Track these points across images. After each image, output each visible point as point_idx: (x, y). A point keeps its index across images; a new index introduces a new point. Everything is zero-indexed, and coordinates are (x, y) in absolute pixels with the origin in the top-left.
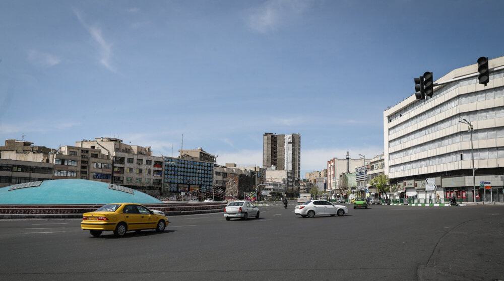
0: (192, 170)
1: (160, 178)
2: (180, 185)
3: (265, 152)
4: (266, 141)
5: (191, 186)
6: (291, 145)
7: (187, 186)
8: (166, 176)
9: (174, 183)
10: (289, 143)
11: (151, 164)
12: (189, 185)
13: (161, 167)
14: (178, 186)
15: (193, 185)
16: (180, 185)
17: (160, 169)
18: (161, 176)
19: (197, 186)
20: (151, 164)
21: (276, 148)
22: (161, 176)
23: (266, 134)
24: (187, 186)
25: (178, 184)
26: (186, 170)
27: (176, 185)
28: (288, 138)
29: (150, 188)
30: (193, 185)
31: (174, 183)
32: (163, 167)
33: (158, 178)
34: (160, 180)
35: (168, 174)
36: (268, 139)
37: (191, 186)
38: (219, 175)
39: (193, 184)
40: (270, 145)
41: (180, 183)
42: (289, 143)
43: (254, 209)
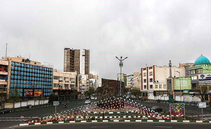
0: (36, 75)
1: (6, 83)
2: (25, 90)
3: (66, 61)
4: (66, 54)
5: (35, 90)
6: (84, 57)
7: (32, 90)
8: (12, 81)
9: (20, 88)
10: (83, 55)
11: (152, 69)
12: (34, 89)
13: (7, 71)
14: (23, 90)
15: (38, 89)
16: (25, 90)
17: (6, 73)
18: (6, 81)
19: (40, 90)
20: (152, 69)
21: (74, 59)
22: (6, 81)
23: (66, 49)
24: (32, 90)
25: (23, 89)
26: (38, 75)
27: (21, 90)
28: (82, 53)
29: (56, 91)
30: (38, 89)
31: (20, 88)
32: (9, 72)
33: (3, 83)
34: (5, 86)
35: (14, 79)
36: (67, 52)
37: (35, 90)
38: (57, 79)
39: (37, 89)
40: (69, 57)
41: (26, 88)
42: (83, 55)
43: (159, 98)
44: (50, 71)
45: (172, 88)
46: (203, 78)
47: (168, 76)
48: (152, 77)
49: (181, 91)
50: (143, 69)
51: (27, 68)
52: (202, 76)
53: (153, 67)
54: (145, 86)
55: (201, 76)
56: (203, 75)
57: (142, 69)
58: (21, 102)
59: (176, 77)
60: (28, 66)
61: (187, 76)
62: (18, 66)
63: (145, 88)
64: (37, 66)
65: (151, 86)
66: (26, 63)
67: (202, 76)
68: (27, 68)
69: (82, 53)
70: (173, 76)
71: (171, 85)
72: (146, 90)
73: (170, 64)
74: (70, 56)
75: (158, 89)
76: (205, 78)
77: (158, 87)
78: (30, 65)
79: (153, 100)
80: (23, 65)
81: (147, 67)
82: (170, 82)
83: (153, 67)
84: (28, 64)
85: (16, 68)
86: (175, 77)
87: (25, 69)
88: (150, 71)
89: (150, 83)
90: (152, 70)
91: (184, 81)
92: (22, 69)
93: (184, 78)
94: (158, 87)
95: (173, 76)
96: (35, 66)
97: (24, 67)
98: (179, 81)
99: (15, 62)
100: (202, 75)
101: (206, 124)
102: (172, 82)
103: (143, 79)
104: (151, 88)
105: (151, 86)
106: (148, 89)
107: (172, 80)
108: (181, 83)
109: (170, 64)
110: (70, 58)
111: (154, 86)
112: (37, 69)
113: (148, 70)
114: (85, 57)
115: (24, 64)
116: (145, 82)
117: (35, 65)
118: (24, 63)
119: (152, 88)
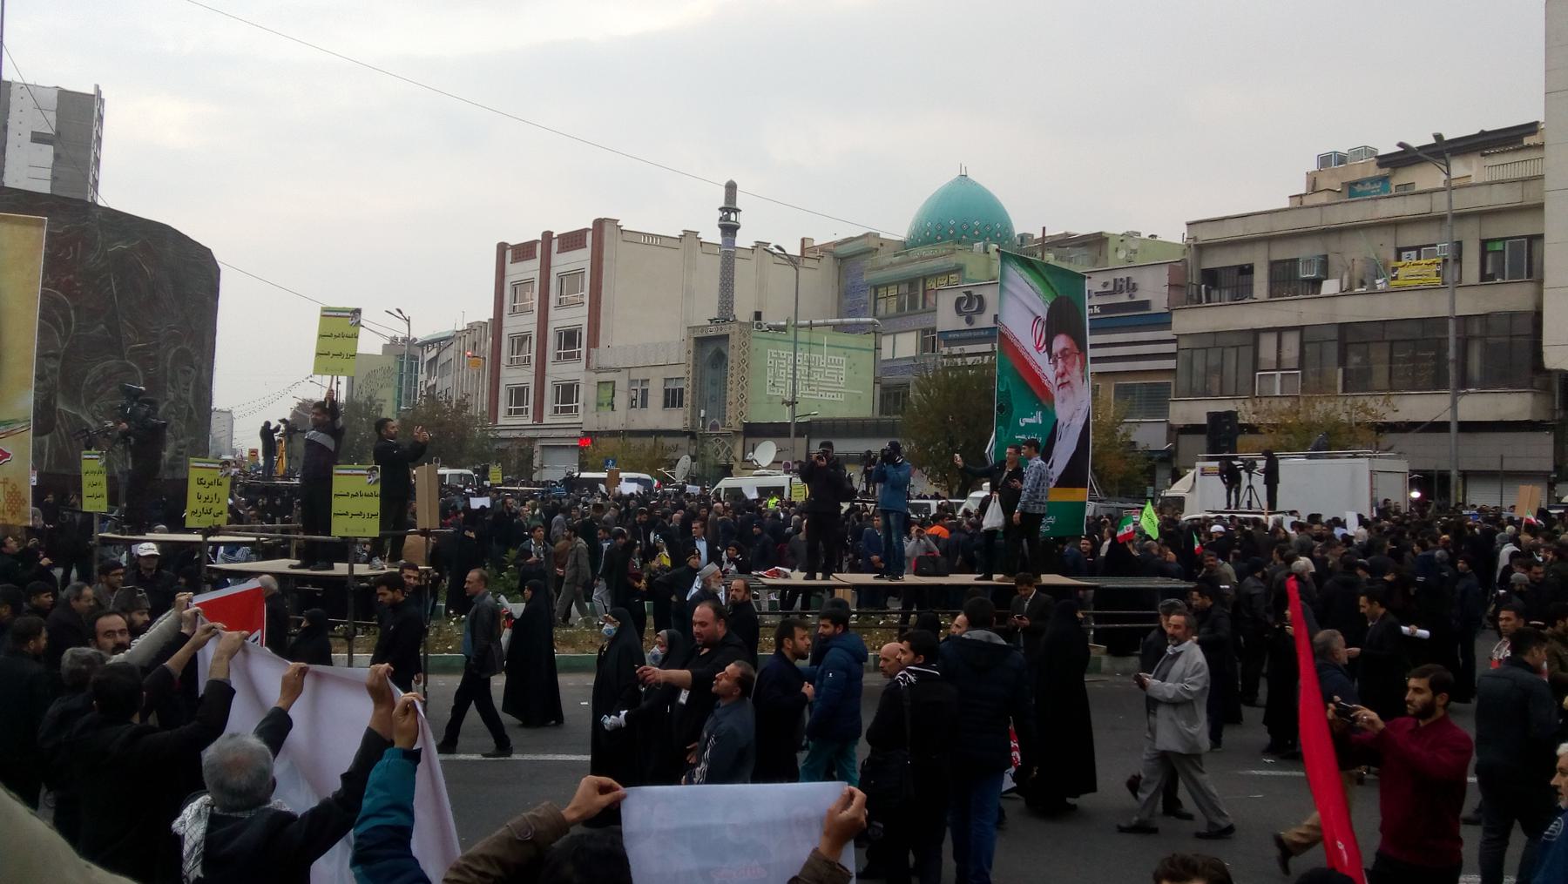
6: (49, 150)
10: (38, 138)
42: (38, 138)
45: (731, 411)
46: (969, 321)
47: (705, 311)
48: (577, 317)
49: (799, 434)
50: (509, 254)
52: (969, 305)
53: (539, 246)
54: (518, 394)
55: (959, 301)
56: (976, 292)
57: (502, 248)
58: (894, 334)
59: (768, 319)
61: (851, 313)
63: (518, 412)
65: (568, 392)
67: (969, 305)
70: (743, 313)
71: (721, 384)
72: (522, 428)
73: (730, 208)
75: (618, 419)
77: (621, 400)
81: (548, 236)
82: (720, 360)
83: (539, 246)
86: (758, 315)
88: (563, 262)
89: (559, 372)
90: (581, 259)
91: (823, 357)
93: (826, 338)
94: (621, 400)
95: (743, 313)
98: (786, 352)
100: (969, 293)
101: (546, 753)
102: (733, 355)
103: (505, 333)
104: (564, 410)
105: (568, 392)
106: (539, 413)
107: (734, 340)
108: (802, 369)
109: (730, 208)
111: (586, 394)
113: (508, 266)
114: (57, 156)
116: (571, 356)
119: (569, 410)
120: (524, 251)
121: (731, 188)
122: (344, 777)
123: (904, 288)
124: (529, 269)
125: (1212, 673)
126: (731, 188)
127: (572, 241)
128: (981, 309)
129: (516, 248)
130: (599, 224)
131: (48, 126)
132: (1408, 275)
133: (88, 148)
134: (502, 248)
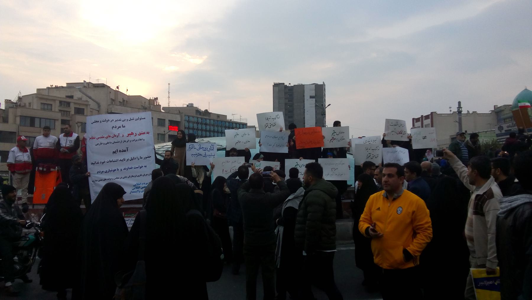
10: (311, 97)
42: (311, 97)
44: (345, 182)
51: (206, 124)
57: (413, 119)
60: (208, 122)
62: (194, 123)
64: (222, 121)
66: (205, 117)
68: (206, 124)
69: (308, 94)
74: (285, 99)
76: (503, 132)
78: (210, 120)
79: (462, 184)
80: (200, 120)
81: (422, 116)
84: (207, 118)
85: (191, 125)
87: (204, 127)
92: (200, 126)
96: (218, 121)
97: (202, 124)
99: (189, 117)
110: (286, 104)
112: (221, 126)
114: (316, 101)
115: (202, 119)
117: (219, 119)
118: (202, 117)
120: (417, 120)
121: (459, 103)
122: (41, 284)
123: (53, 110)
124: (419, 124)
125: (434, 233)
126: (459, 103)
127: (427, 117)
128: (503, 129)
129: (416, 119)
130: (432, 113)
131: (313, 94)
132: (484, 92)
133: (323, 98)
134: (413, 119)
